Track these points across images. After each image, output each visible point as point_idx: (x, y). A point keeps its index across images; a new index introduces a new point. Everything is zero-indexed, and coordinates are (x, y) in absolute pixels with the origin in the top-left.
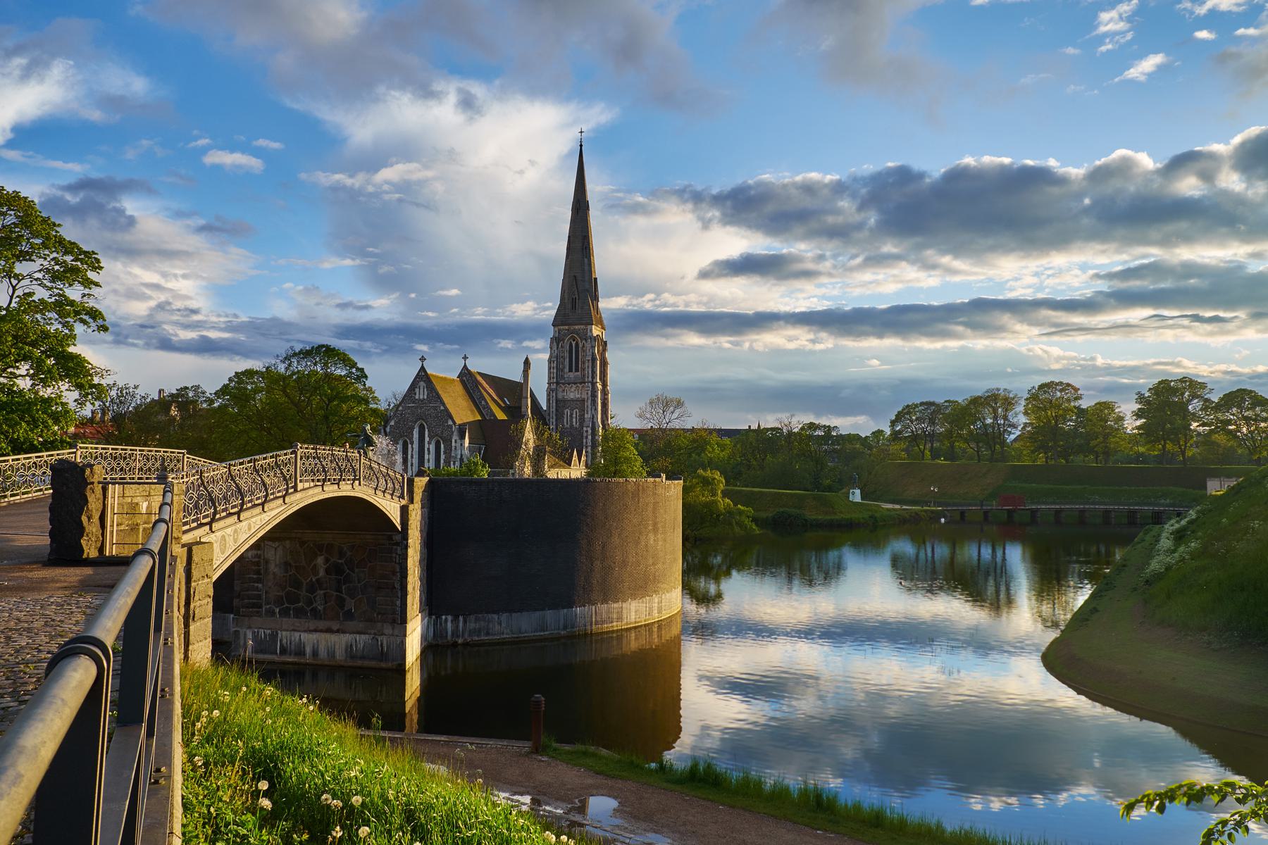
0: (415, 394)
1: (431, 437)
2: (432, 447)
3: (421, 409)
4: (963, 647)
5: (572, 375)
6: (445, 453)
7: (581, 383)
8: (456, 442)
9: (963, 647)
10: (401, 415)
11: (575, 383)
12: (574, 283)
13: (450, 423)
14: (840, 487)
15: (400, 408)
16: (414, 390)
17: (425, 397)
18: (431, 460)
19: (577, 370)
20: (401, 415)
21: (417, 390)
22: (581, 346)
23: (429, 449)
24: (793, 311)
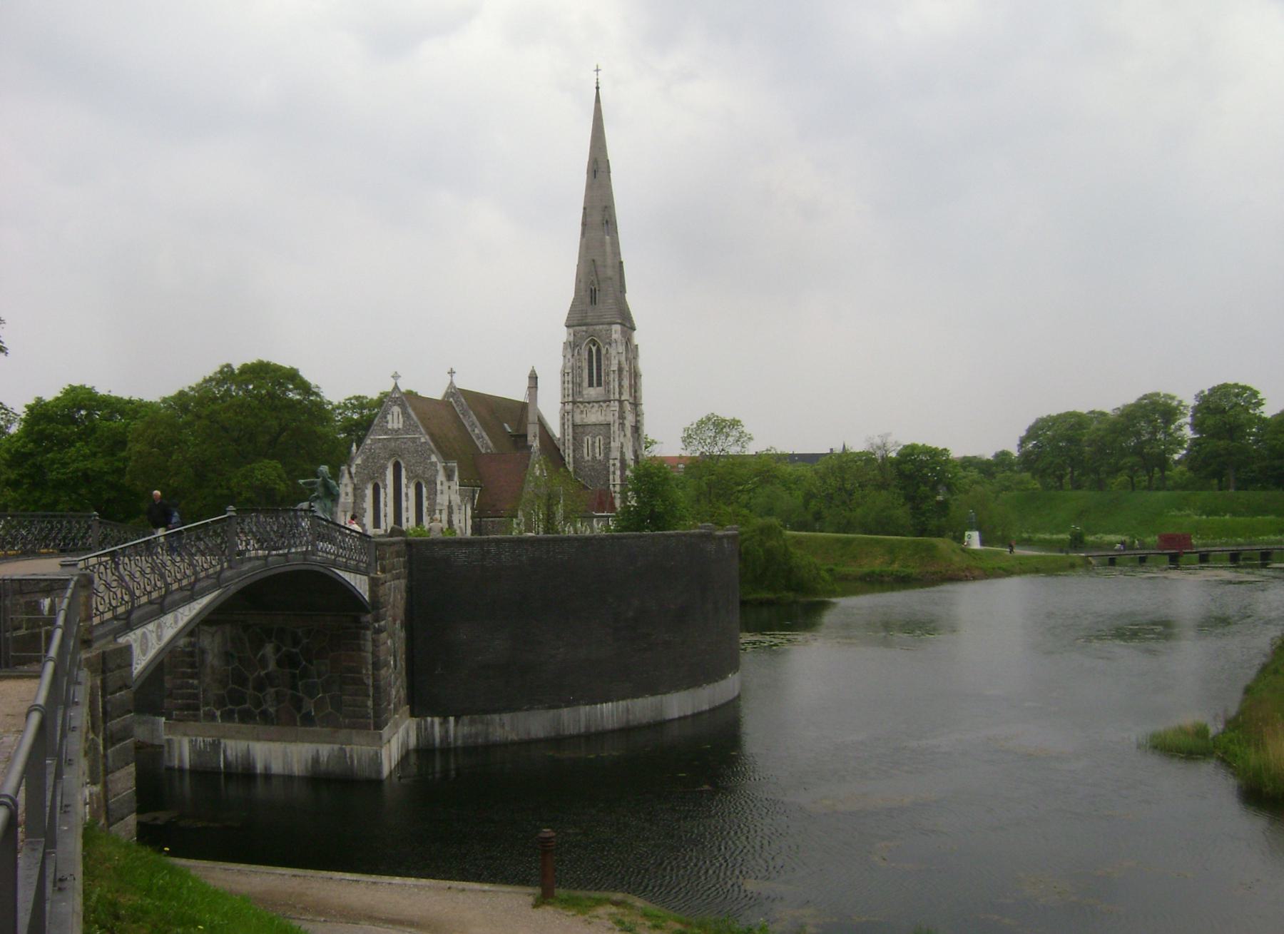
0: (387, 422)
1: (409, 479)
16: (386, 418)
17: (401, 426)
20: (370, 450)
21: (389, 417)
23: (407, 494)
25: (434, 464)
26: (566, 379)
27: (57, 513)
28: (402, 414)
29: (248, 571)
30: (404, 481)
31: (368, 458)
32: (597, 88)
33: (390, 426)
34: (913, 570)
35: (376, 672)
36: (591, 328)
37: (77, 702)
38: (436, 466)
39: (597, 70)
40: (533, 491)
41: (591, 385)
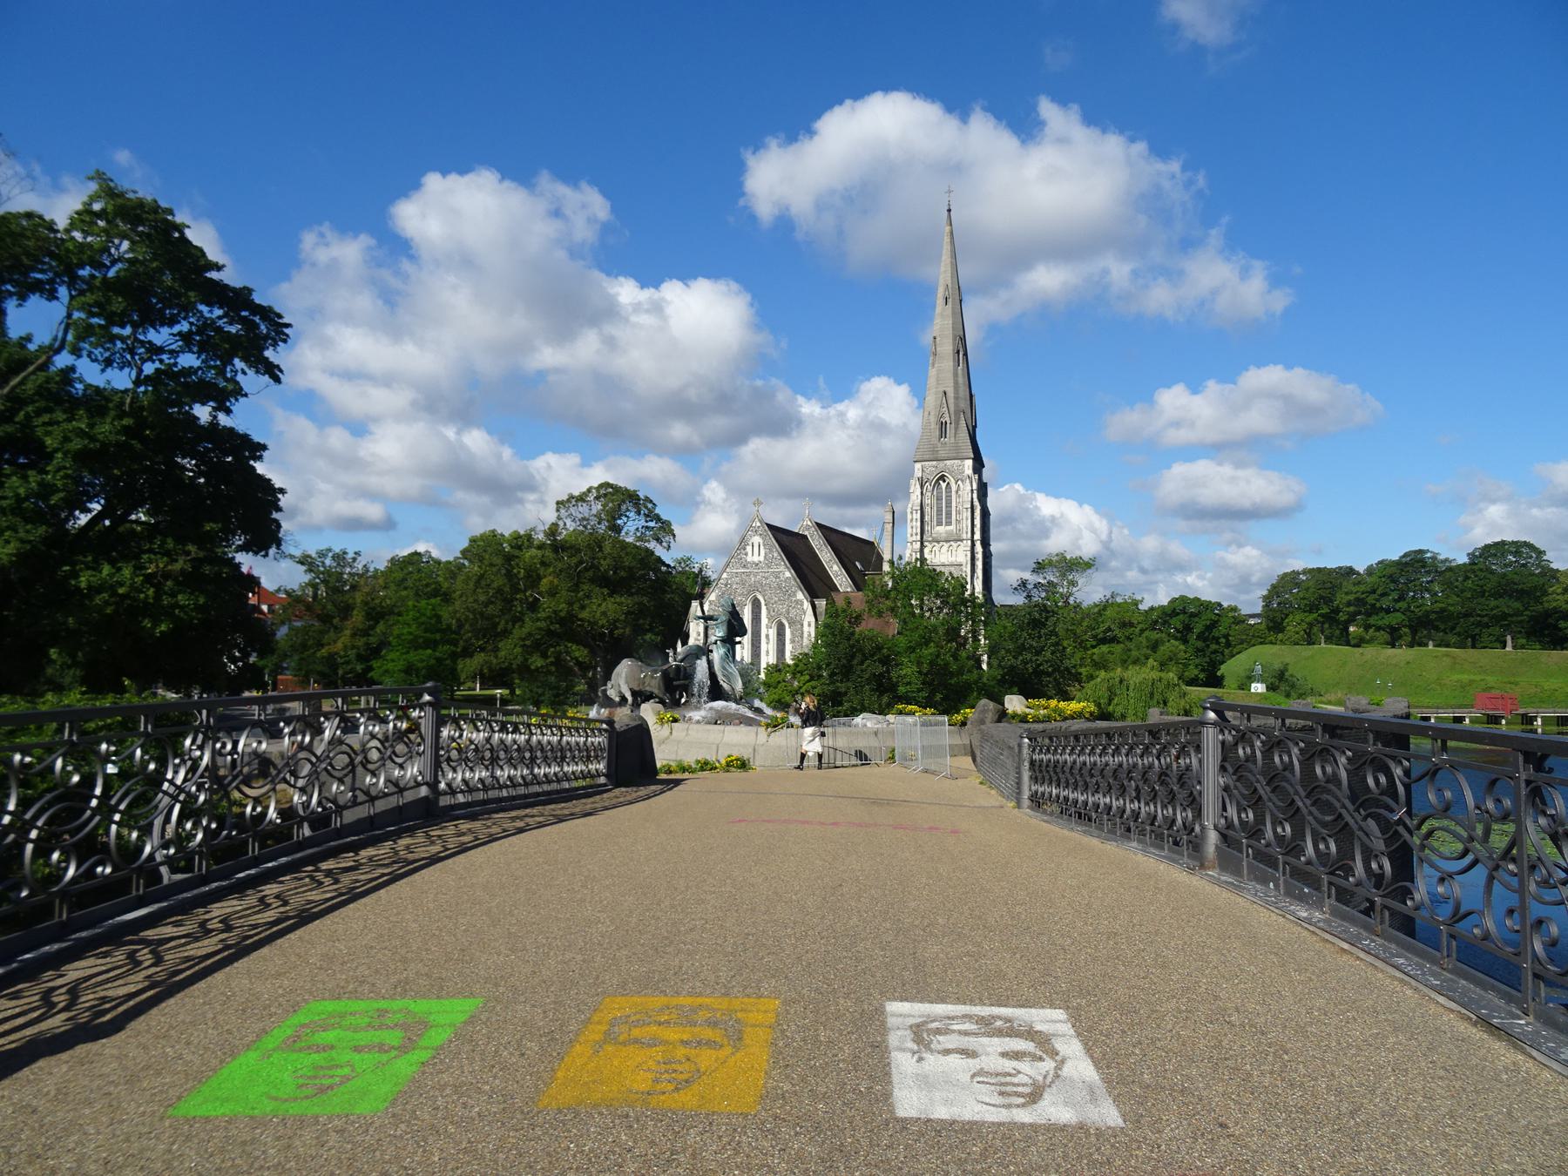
0: (746, 554)
1: (770, 618)
2: (773, 633)
3: (756, 576)
4: (488, 702)
5: (940, 529)
6: (793, 641)
7: (956, 541)
8: (809, 625)
9: (488, 702)
10: (726, 585)
11: (947, 541)
12: (944, 401)
13: (664, 569)
14: (17, 406)
15: (725, 575)
16: (745, 549)
17: (762, 558)
18: (771, 653)
19: (949, 523)
20: (726, 585)
21: (749, 549)
22: (954, 488)
23: (767, 636)
24: (1241, 473)
25: (800, 603)
26: (915, 517)
27: (326, 889)
28: (764, 545)
29: (548, 779)
30: (764, 620)
31: (723, 594)
32: (949, 210)
33: (749, 558)
34: (978, 759)
35: (377, 1049)
36: (941, 464)
37: (1542, 755)
38: (802, 605)
39: (950, 192)
40: (496, 978)
41: (939, 523)
